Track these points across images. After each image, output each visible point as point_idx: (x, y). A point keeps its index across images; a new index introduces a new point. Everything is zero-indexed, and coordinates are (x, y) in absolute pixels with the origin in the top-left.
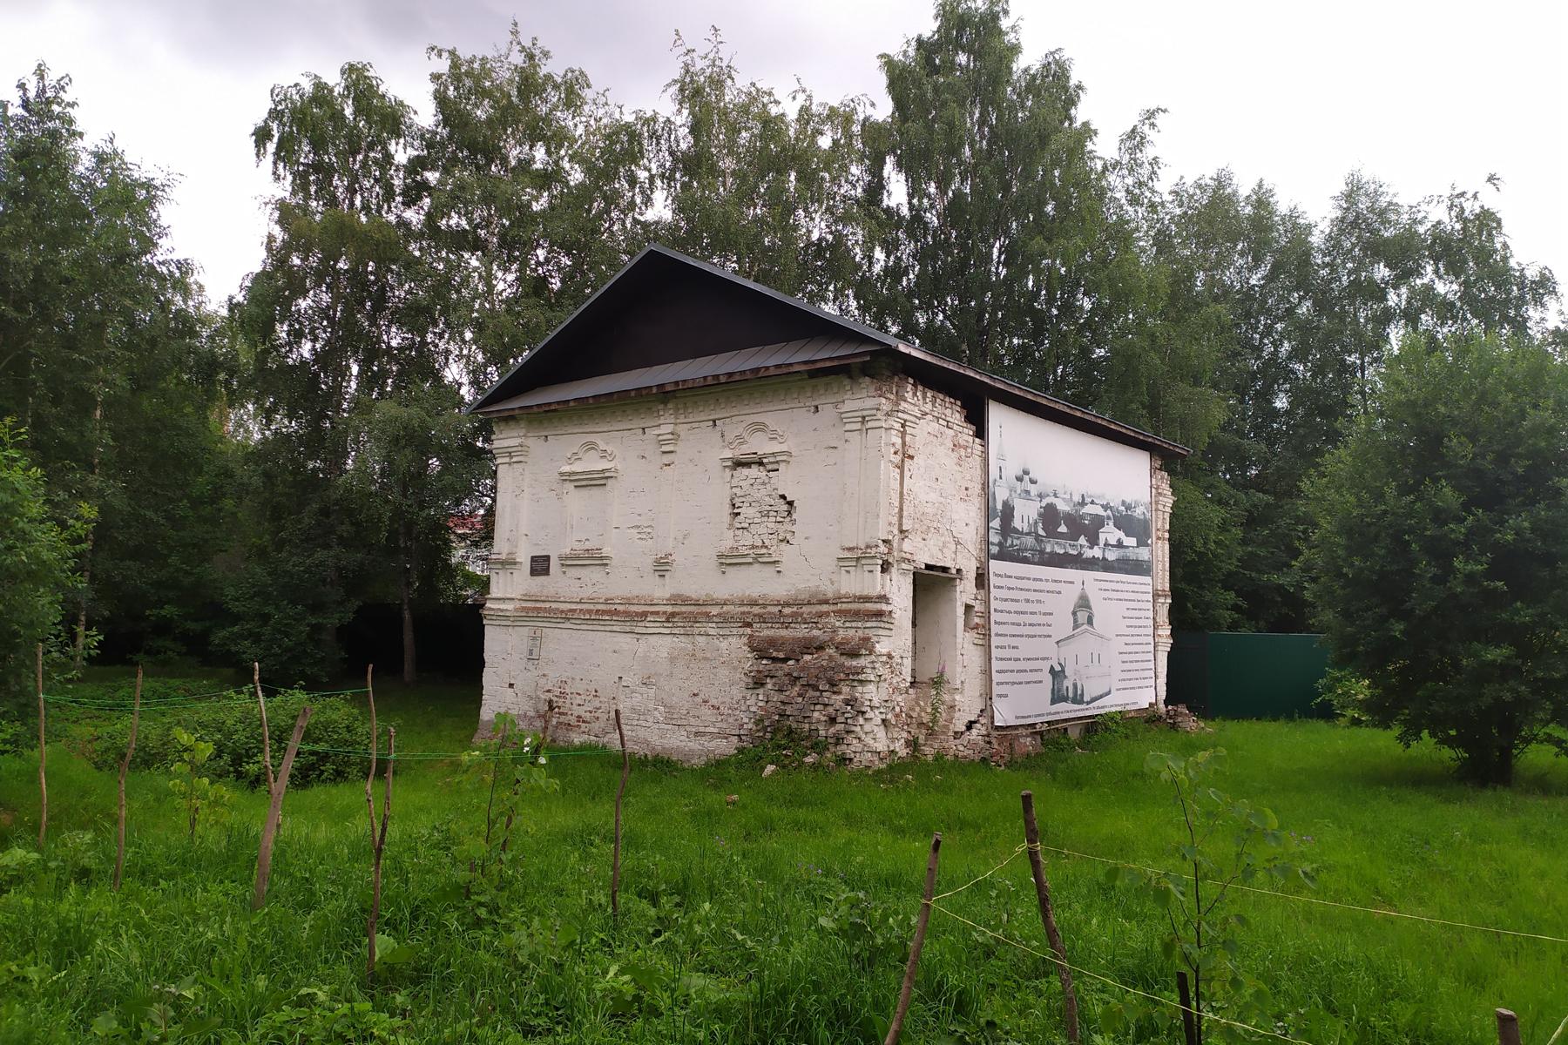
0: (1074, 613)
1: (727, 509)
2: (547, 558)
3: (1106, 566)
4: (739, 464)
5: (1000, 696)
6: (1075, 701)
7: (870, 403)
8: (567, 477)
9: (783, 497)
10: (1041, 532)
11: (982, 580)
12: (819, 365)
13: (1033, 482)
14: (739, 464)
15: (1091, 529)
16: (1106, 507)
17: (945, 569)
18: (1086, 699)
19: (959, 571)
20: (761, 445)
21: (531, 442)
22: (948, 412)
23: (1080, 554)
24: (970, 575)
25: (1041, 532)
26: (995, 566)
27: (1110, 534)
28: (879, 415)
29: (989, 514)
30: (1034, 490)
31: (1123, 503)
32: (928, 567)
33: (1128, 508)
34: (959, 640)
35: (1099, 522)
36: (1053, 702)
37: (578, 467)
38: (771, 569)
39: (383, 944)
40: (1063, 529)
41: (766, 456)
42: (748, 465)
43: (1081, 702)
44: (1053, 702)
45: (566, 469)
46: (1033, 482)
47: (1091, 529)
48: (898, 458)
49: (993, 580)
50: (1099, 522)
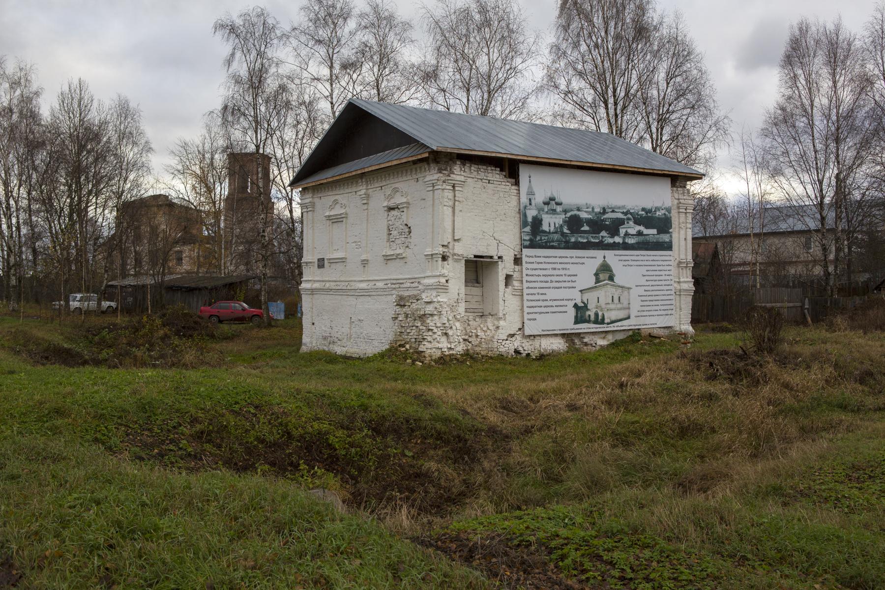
0: (596, 275)
1: (386, 231)
2: (323, 259)
3: (625, 246)
4: (391, 209)
5: (530, 320)
6: (596, 322)
7: (436, 176)
8: (329, 218)
9: (406, 225)
10: (566, 230)
11: (517, 261)
12: (344, 176)
13: (557, 204)
14: (391, 209)
15: (614, 227)
16: (625, 214)
17: (491, 257)
18: (607, 321)
19: (500, 258)
20: (398, 200)
21: (316, 200)
22: (490, 175)
23: (601, 242)
24: (509, 258)
25: (566, 230)
26: (526, 251)
27: (633, 229)
28: (440, 183)
29: (524, 223)
30: (559, 209)
31: (643, 209)
32: (475, 256)
33: (650, 211)
34: (501, 294)
35: (619, 223)
36: (576, 322)
37: (332, 213)
38: (402, 261)
39: (439, 543)
40: (586, 228)
41: (399, 204)
42: (393, 209)
43: (602, 322)
44: (576, 322)
45: (327, 214)
46: (557, 204)
47: (614, 227)
48: (451, 203)
49: (524, 259)
50: (619, 223)
